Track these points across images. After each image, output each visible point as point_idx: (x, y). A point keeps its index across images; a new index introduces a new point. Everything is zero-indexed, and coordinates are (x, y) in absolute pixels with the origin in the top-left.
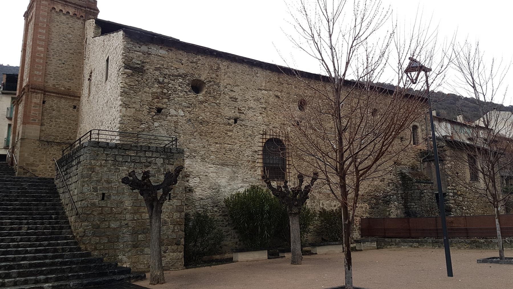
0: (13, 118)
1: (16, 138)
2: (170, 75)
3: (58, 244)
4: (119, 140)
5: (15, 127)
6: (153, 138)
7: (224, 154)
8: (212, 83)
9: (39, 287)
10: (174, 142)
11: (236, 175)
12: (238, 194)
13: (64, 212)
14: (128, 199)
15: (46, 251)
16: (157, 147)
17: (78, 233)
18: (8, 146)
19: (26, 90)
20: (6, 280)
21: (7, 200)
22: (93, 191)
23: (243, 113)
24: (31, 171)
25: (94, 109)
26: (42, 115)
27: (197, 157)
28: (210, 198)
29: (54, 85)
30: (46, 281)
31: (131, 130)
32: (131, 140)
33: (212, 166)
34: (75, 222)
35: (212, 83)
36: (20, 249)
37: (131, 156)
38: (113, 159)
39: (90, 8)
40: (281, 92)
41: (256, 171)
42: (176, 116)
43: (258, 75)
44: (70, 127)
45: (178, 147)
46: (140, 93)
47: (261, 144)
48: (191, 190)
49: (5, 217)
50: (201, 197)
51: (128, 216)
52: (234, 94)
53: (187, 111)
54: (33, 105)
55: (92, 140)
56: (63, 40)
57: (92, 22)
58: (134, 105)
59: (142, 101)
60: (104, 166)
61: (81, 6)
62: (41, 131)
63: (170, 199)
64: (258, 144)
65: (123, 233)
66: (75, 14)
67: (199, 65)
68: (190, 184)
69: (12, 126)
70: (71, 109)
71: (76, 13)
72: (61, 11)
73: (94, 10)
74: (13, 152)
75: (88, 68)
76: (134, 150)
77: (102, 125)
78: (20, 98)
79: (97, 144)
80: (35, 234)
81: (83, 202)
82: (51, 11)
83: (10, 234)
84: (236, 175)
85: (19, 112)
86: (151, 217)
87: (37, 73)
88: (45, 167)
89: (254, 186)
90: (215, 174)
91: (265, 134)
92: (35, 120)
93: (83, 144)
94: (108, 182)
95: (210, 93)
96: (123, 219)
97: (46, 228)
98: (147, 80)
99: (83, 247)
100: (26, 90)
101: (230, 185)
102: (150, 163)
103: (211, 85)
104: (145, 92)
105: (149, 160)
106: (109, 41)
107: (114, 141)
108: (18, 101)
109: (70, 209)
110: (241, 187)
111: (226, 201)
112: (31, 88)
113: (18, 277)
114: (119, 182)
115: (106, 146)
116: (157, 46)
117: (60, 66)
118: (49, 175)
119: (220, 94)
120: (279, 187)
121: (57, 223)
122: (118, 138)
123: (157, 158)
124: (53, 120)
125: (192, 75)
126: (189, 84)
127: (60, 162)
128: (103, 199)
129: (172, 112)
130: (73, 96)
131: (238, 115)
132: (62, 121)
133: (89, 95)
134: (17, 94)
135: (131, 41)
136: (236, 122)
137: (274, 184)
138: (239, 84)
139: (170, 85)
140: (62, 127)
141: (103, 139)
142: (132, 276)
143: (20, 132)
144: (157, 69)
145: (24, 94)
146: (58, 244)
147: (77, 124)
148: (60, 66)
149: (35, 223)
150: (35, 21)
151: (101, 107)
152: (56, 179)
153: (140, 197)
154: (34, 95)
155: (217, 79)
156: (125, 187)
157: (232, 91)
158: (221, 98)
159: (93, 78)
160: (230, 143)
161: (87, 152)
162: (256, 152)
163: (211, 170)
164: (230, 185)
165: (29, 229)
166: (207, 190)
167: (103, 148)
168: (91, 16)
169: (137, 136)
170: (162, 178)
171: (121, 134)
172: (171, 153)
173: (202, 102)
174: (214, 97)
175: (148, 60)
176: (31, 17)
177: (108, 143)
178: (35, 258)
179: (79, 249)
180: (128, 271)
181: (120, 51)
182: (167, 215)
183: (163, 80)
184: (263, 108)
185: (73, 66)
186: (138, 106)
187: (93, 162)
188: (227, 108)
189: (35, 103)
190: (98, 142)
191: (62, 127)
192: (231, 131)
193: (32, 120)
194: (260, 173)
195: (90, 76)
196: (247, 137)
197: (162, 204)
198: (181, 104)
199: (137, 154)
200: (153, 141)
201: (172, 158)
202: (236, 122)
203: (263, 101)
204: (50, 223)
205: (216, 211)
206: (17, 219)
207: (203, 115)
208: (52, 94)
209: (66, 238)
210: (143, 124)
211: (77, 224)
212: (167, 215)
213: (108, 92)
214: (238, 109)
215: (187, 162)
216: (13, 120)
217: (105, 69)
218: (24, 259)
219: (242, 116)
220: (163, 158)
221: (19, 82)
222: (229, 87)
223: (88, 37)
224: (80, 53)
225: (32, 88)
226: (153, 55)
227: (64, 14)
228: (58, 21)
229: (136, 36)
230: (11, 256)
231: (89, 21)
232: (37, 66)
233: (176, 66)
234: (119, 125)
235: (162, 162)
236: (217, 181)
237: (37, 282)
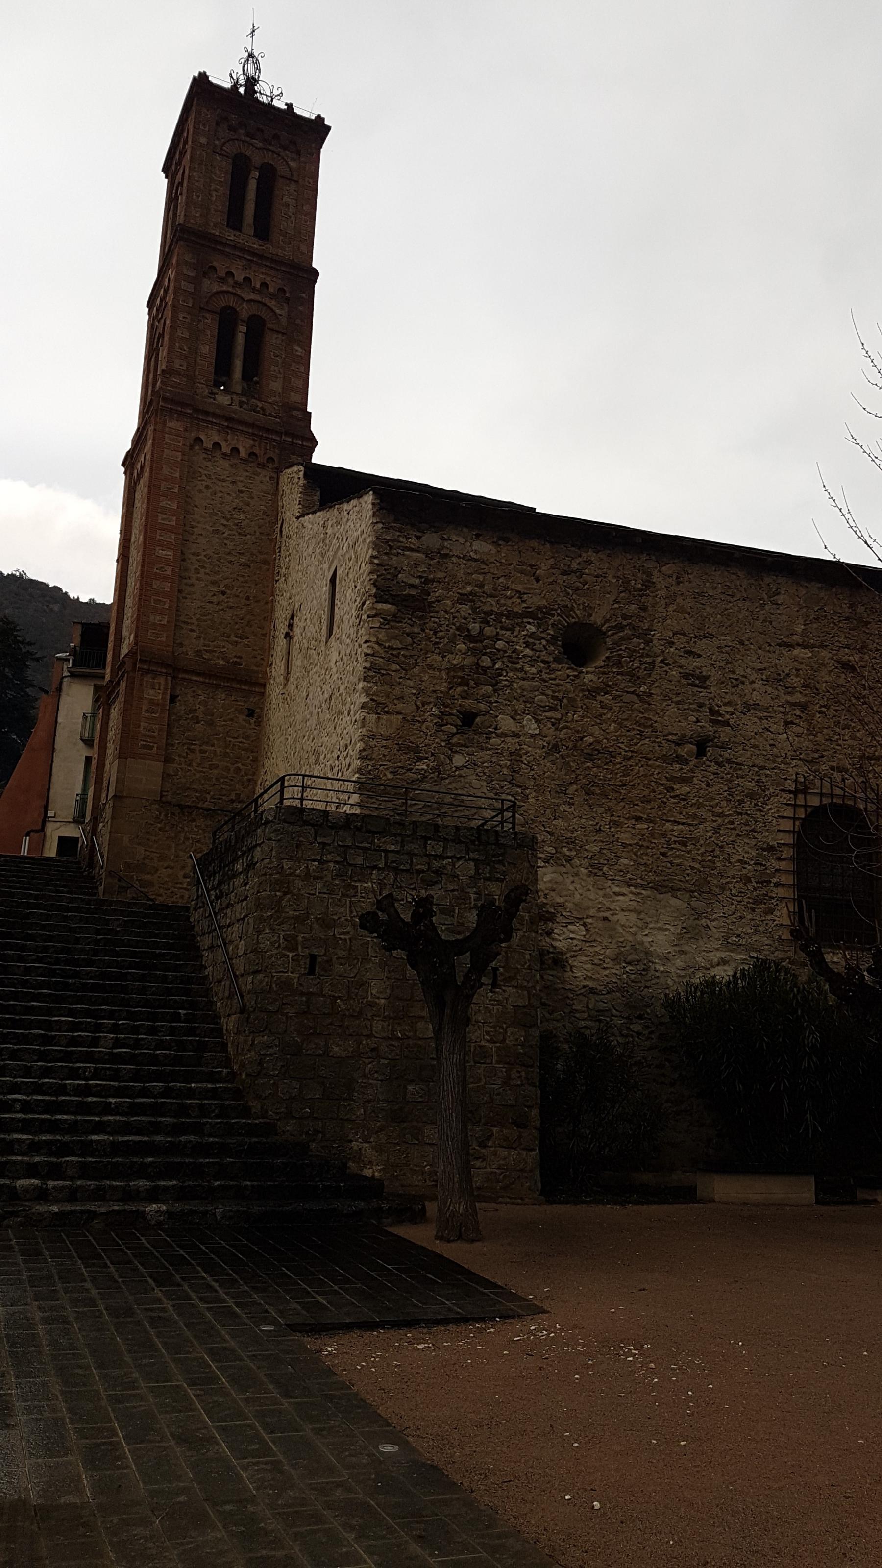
0: (97, 741)
1: (104, 795)
2: (501, 614)
3: (191, 1094)
4: (358, 804)
5: (101, 766)
6: (448, 799)
7: (664, 854)
8: (628, 631)
9: (132, 1212)
10: (508, 815)
11: (703, 922)
12: (712, 984)
13: (212, 1003)
14: (379, 977)
15: (157, 1109)
16: (457, 828)
17: (243, 1066)
18: (84, 816)
19: (128, 666)
20: (51, 1183)
21: (67, 962)
22: (286, 948)
23: (727, 723)
24: (137, 884)
25: (299, 717)
26: (169, 734)
27: (576, 861)
28: (619, 990)
29: (198, 653)
30: (153, 1196)
31: (390, 776)
32: (389, 805)
33: (625, 890)
34: (238, 1033)
35: (628, 631)
36: (89, 1099)
37: (386, 851)
38: (338, 859)
39: (293, 436)
40: (863, 649)
41: (770, 911)
42: (516, 735)
43: (780, 599)
44: (239, 769)
45: (518, 828)
46: (416, 670)
47: (788, 825)
48: (558, 961)
49: (60, 1008)
50: (590, 984)
51: (378, 1026)
52: (697, 663)
53: (549, 718)
54: (144, 708)
55: (287, 803)
56: (221, 528)
57: (296, 472)
58: (400, 706)
59: (421, 691)
60: (315, 878)
61: (268, 430)
62: (166, 776)
63: (495, 985)
64: (779, 824)
65: (365, 1076)
66: (252, 454)
67: (588, 578)
68: (557, 944)
69: (94, 762)
70: (242, 717)
71: (256, 450)
72: (217, 445)
73: (303, 438)
74: (94, 831)
75: (285, 603)
76: (395, 835)
77: (317, 761)
78: (114, 685)
79: (298, 815)
80: (131, 1059)
81: (260, 976)
82: (191, 447)
83: (67, 1057)
84: (703, 922)
85: (111, 724)
86: (438, 1032)
87: (155, 619)
88: (171, 876)
89: (765, 961)
90: (633, 917)
91: (802, 789)
92: (151, 748)
93: (262, 814)
94: (326, 923)
95: (619, 664)
96: (365, 1032)
97: (160, 1045)
98: (435, 633)
99: (255, 1105)
100: (128, 666)
101: (684, 952)
102: (438, 872)
103: (622, 639)
104: (430, 667)
105: (436, 864)
106: (338, 523)
107: (346, 809)
108: (109, 696)
109: (227, 994)
110: (718, 961)
111: (671, 1004)
112: (141, 661)
113: (80, 1178)
114: (354, 925)
115: (322, 822)
116: (465, 530)
117: (215, 599)
118: (182, 897)
119: (653, 665)
120: (852, 970)
121: (192, 1032)
122: (355, 798)
123: (459, 859)
124: (197, 748)
125: (567, 610)
126: (554, 638)
127: (204, 862)
128: (311, 971)
129: (506, 723)
130: (245, 684)
131: (710, 729)
132: (218, 750)
133: (287, 679)
134: (108, 677)
135: (395, 521)
136: (701, 751)
137: (835, 959)
138: (713, 630)
139: (500, 644)
140: (217, 767)
141: (316, 800)
142: (385, 1206)
143: (113, 779)
144: (463, 599)
145: (123, 676)
146: (191, 1094)
147: (255, 760)
148: (215, 599)
149: (135, 1030)
150: (151, 477)
151: (315, 712)
152: (195, 910)
153: (410, 972)
154: (148, 678)
155: (642, 619)
156: (371, 939)
157: (690, 653)
158: (654, 676)
159: (297, 631)
160: (680, 818)
161: (273, 836)
162: (771, 848)
163: (622, 903)
164: (684, 952)
165: (117, 1043)
166: (609, 963)
167: (313, 825)
168: (294, 458)
169: (406, 793)
170: (472, 918)
171: (362, 787)
172: (502, 848)
173: (593, 693)
174: (633, 676)
175: (440, 575)
176: (142, 468)
177: (326, 813)
178: (126, 1128)
179: (245, 1111)
180: (374, 1188)
181: (365, 552)
182: (488, 1033)
183: (481, 630)
184: (793, 704)
185: (248, 598)
186: (409, 708)
187: (286, 864)
188: (673, 710)
189: (151, 702)
190: (301, 810)
191: (217, 767)
192: (683, 780)
193: (144, 747)
194: (786, 921)
195: (291, 626)
196: (741, 802)
197: (470, 997)
198: (530, 701)
199: (403, 846)
200: (450, 811)
201: (500, 862)
202: (701, 751)
203: (794, 681)
204: (172, 1031)
205: (639, 1034)
206: (88, 1014)
207: (596, 730)
208: (194, 678)
209: (212, 1077)
210: (421, 759)
211: (242, 1038)
212: (488, 1033)
213: (334, 670)
214: (712, 711)
215: (547, 875)
216: (96, 747)
217: (326, 605)
218: (99, 1128)
219: (725, 734)
220: (474, 860)
221: (110, 645)
222: (680, 641)
223: (287, 515)
224: (265, 562)
225: (145, 661)
226: (454, 559)
227: (225, 455)
228: (209, 476)
229: (409, 505)
230: (65, 1117)
231: (289, 471)
232: (156, 601)
233: (520, 587)
234: (358, 762)
235: (472, 872)
236: (639, 937)
237: (128, 1196)
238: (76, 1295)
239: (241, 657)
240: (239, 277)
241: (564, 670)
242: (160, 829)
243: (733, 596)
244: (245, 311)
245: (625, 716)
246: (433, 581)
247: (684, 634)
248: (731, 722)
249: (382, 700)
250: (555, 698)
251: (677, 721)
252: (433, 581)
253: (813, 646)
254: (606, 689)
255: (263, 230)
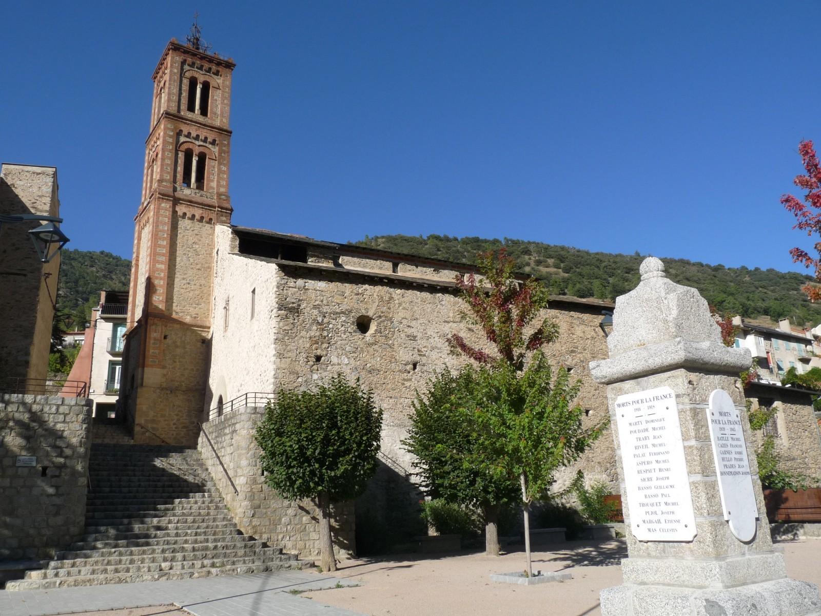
2: (331, 313)
23: (425, 355)
35: (383, 318)
42: (339, 364)
43: (443, 303)
52: (413, 330)
103: (381, 322)
117: (184, 287)
118: (173, 435)
119: (394, 332)
129: (334, 360)
131: (418, 358)
140: (187, 369)
144: (315, 307)
155: (389, 313)
173: (370, 345)
185: (201, 285)
189: (155, 339)
202: (415, 368)
214: (419, 351)
219: (424, 360)
222: (405, 322)
233: (338, 301)
238: (472, 503)
239: (197, 314)
240: (194, 134)
241: (359, 335)
242: (161, 402)
243: (425, 302)
244: (197, 150)
245: (384, 354)
246: (302, 300)
247: (406, 319)
248: (426, 355)
249: (282, 352)
250: (355, 348)
251: (405, 355)
252: (302, 300)
253: (457, 322)
254: (375, 343)
255: (204, 112)
